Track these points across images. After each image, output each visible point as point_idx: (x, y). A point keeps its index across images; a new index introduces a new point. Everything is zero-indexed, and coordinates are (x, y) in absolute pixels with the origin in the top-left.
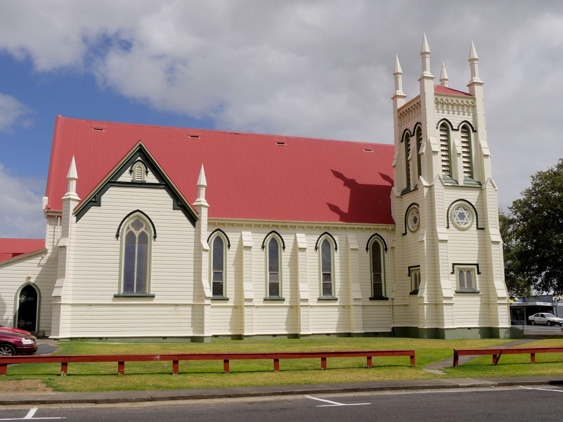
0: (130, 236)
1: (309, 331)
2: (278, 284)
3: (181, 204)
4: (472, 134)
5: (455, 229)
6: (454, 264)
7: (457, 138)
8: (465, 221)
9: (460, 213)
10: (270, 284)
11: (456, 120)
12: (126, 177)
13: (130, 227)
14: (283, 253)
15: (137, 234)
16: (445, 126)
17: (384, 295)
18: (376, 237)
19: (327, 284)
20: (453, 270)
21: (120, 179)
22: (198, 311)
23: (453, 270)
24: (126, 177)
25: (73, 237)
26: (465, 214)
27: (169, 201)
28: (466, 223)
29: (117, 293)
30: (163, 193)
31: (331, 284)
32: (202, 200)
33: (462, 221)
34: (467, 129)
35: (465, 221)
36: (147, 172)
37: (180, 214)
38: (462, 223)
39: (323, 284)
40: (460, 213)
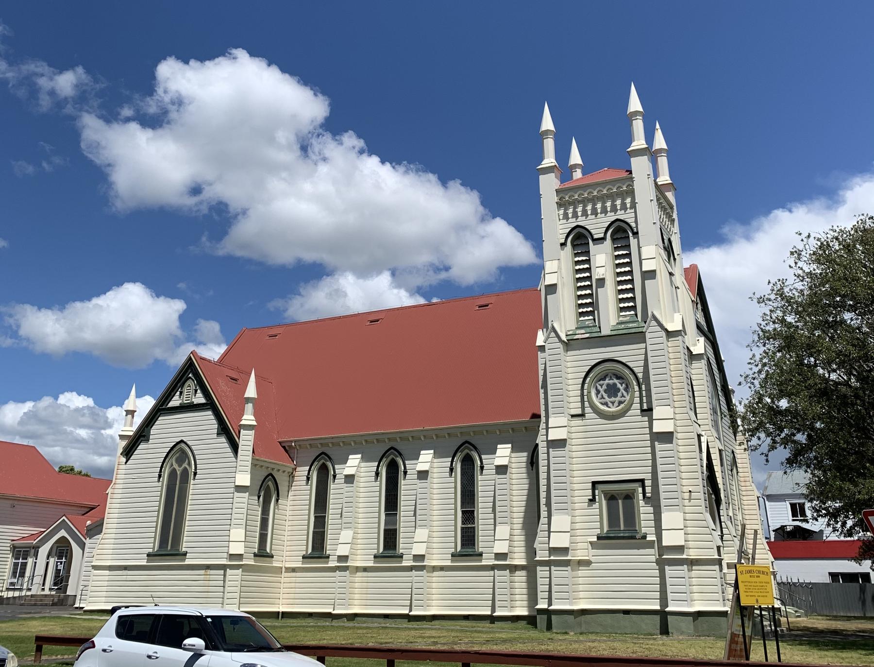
0: (173, 473)
1: (571, 604)
2: (396, 530)
3: (224, 430)
4: (633, 241)
5: (594, 415)
6: (594, 484)
7: (602, 258)
8: (618, 399)
9: (608, 385)
10: (385, 530)
11: (597, 225)
12: (175, 402)
13: (174, 463)
14: (332, 486)
15: (179, 470)
16: (580, 239)
17: (268, 550)
18: (467, 448)
19: (390, 530)
20: (594, 495)
21: (172, 404)
22: (514, 568)
23: (594, 495)
24: (175, 402)
25: (435, 475)
26: (619, 385)
27: (214, 424)
28: (606, 404)
29: (151, 550)
30: (209, 414)
31: (474, 528)
32: (248, 418)
33: (613, 399)
34: (621, 234)
35: (618, 399)
36: (196, 391)
37: (223, 439)
38: (613, 403)
39: (462, 529)
40: (608, 385)
